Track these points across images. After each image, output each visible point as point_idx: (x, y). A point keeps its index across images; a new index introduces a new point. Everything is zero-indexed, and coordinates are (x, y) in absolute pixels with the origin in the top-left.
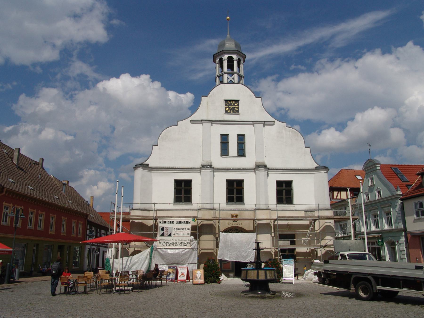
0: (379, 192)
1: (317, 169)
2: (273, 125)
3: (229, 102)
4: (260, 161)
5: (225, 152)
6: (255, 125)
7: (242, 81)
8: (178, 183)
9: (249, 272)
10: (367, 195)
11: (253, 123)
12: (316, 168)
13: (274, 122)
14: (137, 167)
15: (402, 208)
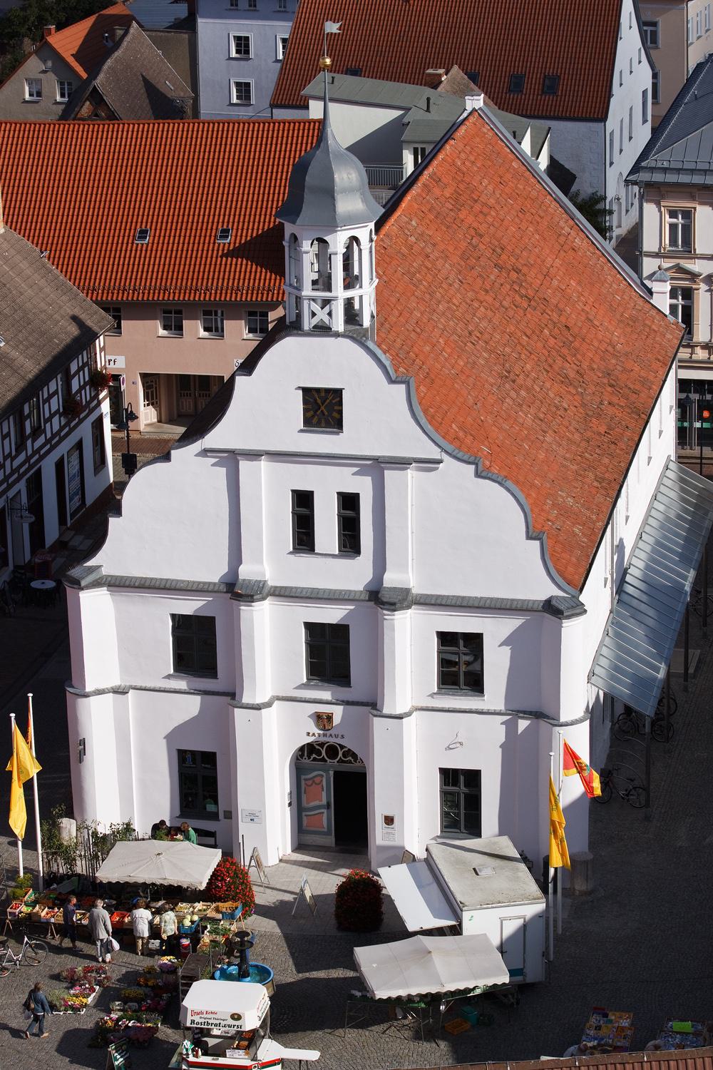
5: (304, 538)
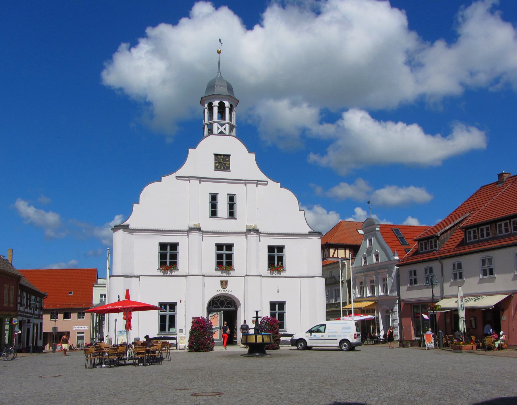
0: (377, 256)
1: (311, 234)
2: (266, 185)
4: (252, 224)
8: (163, 246)
9: (249, 336)
10: (365, 258)
11: (246, 182)
12: (309, 232)
13: (267, 181)
14: (116, 228)
15: (398, 275)
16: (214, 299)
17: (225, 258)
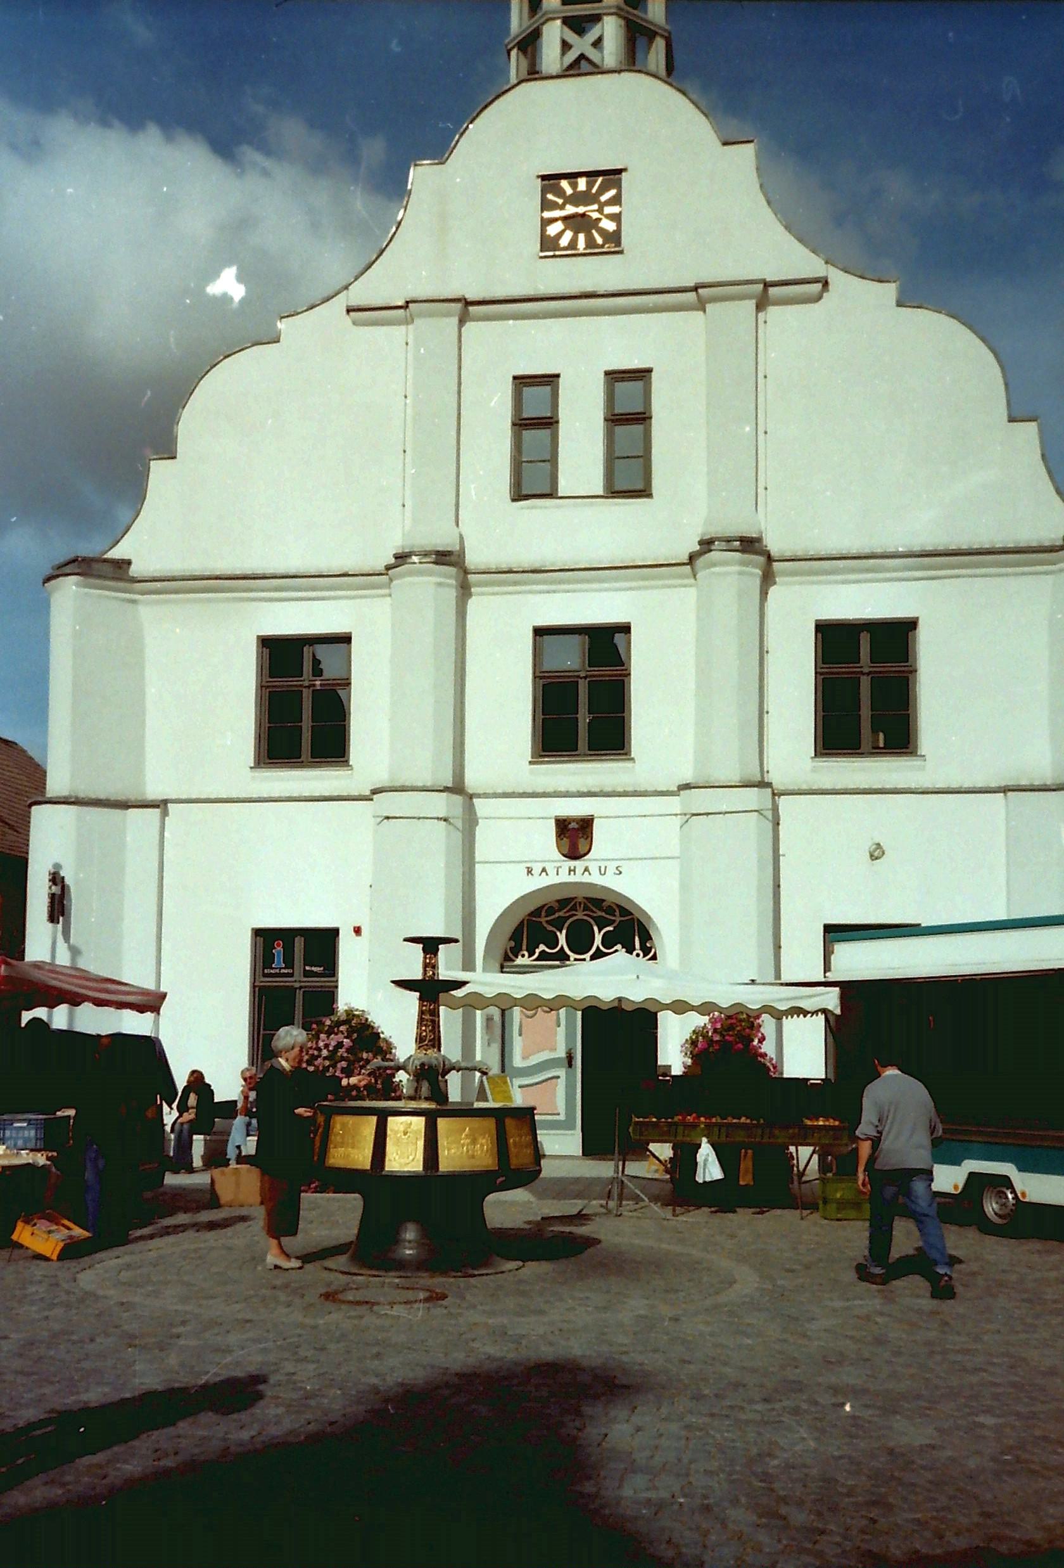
3: (564, 184)
6: (709, 307)
7: (657, 54)
11: (699, 295)
16: (537, 912)
17: (583, 700)
